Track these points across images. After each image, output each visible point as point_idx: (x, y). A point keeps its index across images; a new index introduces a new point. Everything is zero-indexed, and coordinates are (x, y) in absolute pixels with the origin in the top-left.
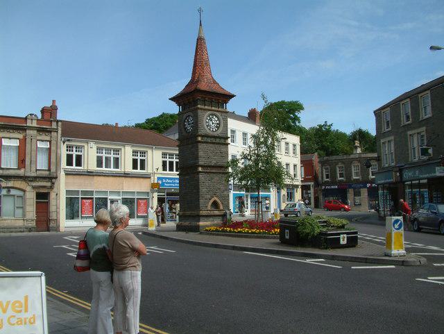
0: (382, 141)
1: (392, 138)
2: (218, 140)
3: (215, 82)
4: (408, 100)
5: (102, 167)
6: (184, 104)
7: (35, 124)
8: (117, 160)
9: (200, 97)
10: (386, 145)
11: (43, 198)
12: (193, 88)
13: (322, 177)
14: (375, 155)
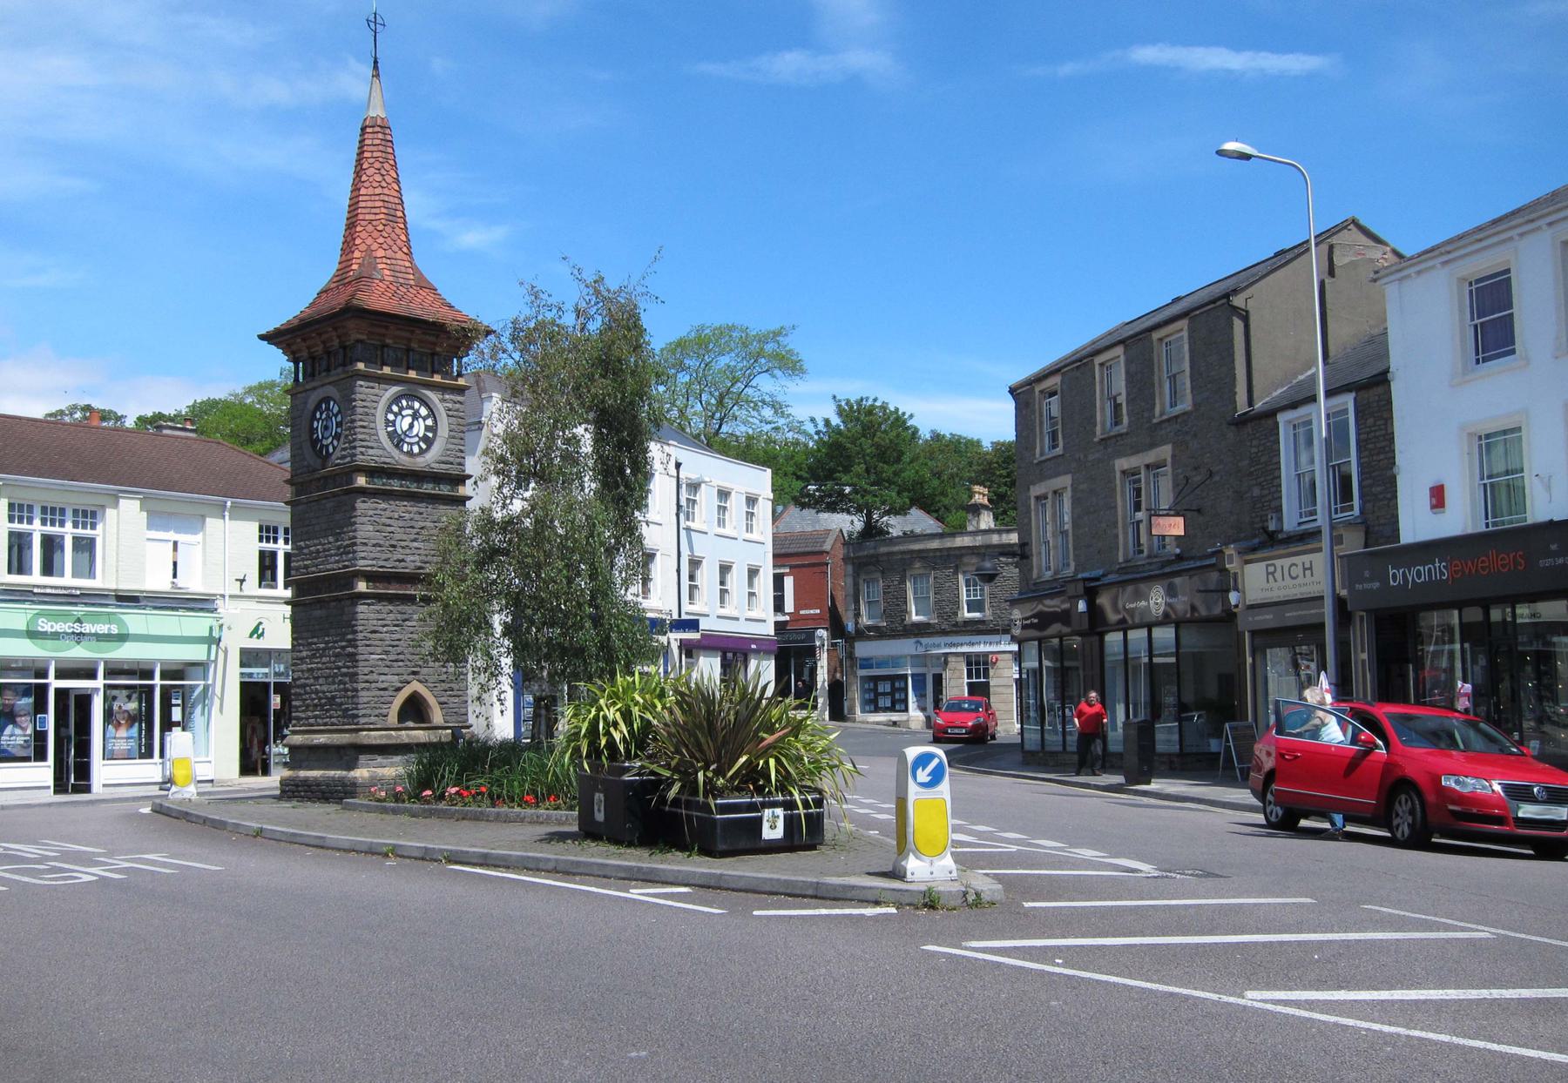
1: (1065, 481)
2: (428, 488)
3: (424, 285)
4: (1119, 350)
5: (275, 587)
6: (313, 358)
8: (85, 547)
9: (356, 339)
10: (1049, 503)
12: (339, 301)
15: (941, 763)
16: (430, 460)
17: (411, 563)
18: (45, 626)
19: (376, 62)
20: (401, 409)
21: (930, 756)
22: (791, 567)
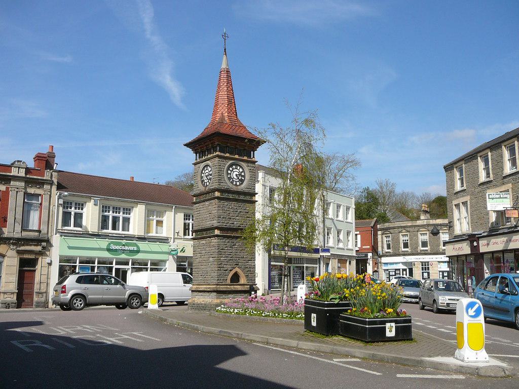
0: (455, 202)
1: (467, 198)
2: (242, 197)
7: (22, 173)
8: (127, 221)
11: (27, 266)
13: (383, 248)
14: (446, 221)
15: (479, 306)
16: (243, 187)
17: (236, 224)
18: (113, 247)
19: (225, 50)
20: (233, 169)
21: (475, 303)
22: (360, 231)
